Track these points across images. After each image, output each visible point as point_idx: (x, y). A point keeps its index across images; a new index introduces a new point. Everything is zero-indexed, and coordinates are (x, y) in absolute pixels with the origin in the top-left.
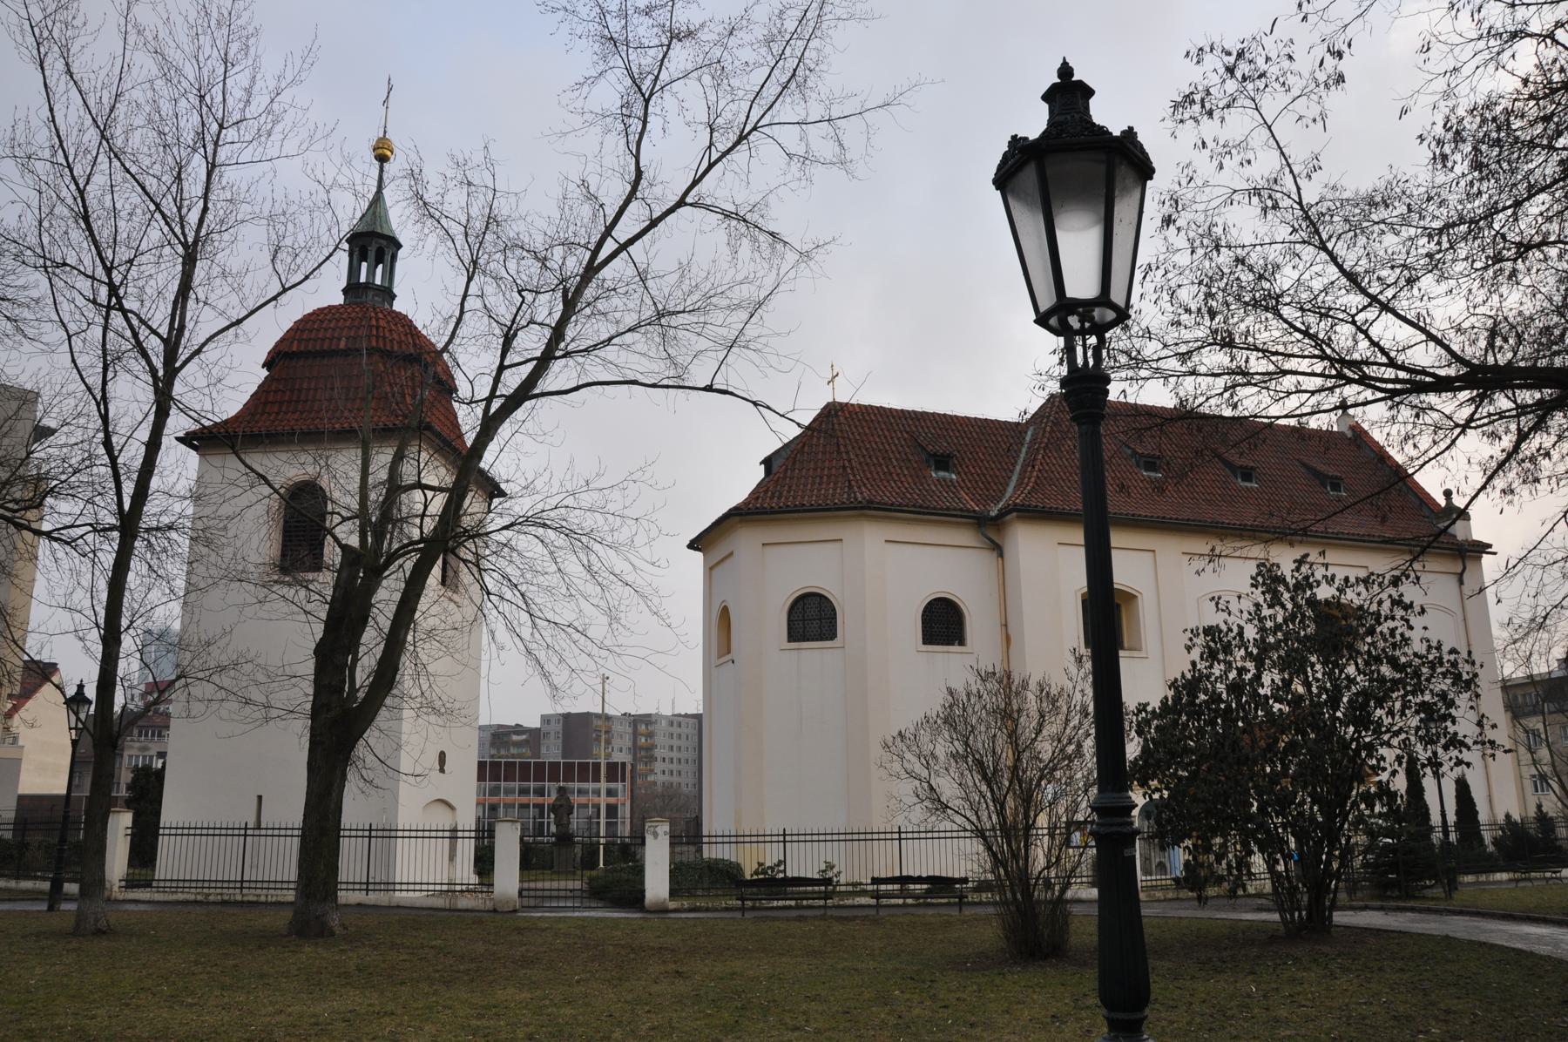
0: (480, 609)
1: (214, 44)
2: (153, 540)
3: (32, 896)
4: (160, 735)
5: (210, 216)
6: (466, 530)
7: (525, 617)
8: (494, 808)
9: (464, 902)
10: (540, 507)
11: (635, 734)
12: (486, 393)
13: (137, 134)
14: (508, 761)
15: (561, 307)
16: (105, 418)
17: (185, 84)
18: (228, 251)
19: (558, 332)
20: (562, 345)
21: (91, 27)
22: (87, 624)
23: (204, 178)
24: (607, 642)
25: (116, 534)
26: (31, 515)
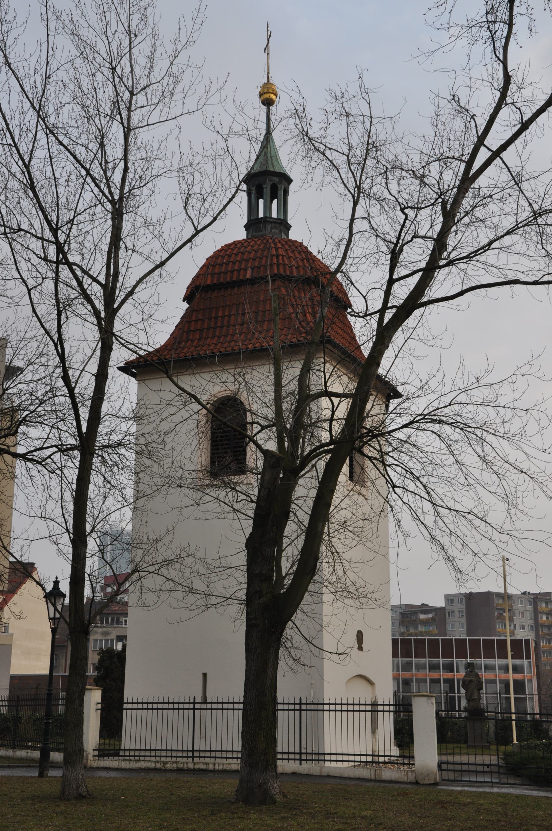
0: (386, 500)
1: (119, 19)
2: (106, 456)
3: (26, 763)
4: (118, 621)
5: (130, 175)
6: (370, 431)
7: (427, 506)
8: (407, 683)
9: (388, 774)
10: (435, 404)
11: (536, 613)
12: (378, 305)
13: (66, 109)
14: (418, 638)
15: (441, 219)
16: (62, 357)
17: (99, 59)
18: (147, 204)
19: (440, 243)
20: (445, 254)
21: (20, 19)
22: (59, 530)
23: (122, 141)
24: (507, 527)
25: (76, 453)
26: (9, 441)
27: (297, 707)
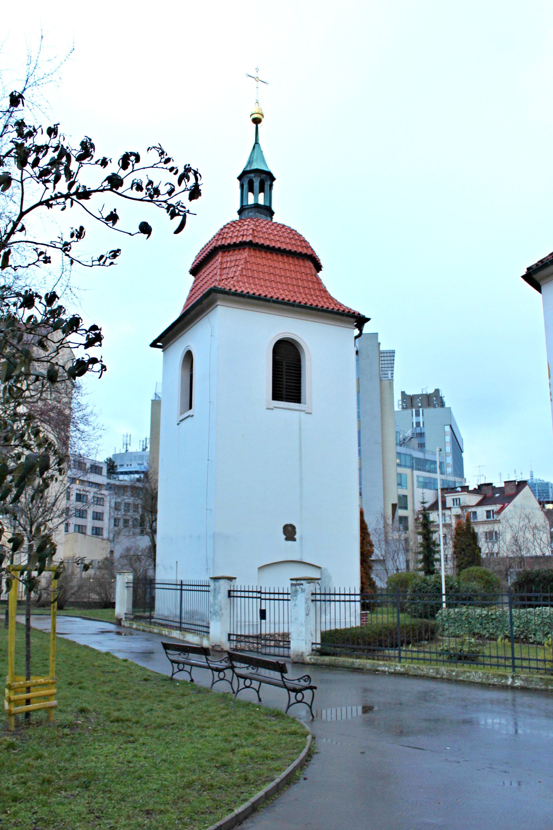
27: (179, 587)
